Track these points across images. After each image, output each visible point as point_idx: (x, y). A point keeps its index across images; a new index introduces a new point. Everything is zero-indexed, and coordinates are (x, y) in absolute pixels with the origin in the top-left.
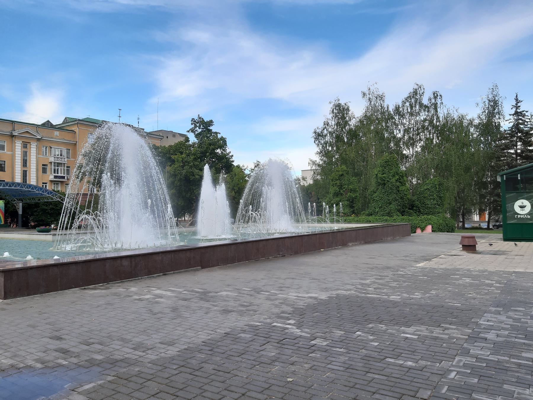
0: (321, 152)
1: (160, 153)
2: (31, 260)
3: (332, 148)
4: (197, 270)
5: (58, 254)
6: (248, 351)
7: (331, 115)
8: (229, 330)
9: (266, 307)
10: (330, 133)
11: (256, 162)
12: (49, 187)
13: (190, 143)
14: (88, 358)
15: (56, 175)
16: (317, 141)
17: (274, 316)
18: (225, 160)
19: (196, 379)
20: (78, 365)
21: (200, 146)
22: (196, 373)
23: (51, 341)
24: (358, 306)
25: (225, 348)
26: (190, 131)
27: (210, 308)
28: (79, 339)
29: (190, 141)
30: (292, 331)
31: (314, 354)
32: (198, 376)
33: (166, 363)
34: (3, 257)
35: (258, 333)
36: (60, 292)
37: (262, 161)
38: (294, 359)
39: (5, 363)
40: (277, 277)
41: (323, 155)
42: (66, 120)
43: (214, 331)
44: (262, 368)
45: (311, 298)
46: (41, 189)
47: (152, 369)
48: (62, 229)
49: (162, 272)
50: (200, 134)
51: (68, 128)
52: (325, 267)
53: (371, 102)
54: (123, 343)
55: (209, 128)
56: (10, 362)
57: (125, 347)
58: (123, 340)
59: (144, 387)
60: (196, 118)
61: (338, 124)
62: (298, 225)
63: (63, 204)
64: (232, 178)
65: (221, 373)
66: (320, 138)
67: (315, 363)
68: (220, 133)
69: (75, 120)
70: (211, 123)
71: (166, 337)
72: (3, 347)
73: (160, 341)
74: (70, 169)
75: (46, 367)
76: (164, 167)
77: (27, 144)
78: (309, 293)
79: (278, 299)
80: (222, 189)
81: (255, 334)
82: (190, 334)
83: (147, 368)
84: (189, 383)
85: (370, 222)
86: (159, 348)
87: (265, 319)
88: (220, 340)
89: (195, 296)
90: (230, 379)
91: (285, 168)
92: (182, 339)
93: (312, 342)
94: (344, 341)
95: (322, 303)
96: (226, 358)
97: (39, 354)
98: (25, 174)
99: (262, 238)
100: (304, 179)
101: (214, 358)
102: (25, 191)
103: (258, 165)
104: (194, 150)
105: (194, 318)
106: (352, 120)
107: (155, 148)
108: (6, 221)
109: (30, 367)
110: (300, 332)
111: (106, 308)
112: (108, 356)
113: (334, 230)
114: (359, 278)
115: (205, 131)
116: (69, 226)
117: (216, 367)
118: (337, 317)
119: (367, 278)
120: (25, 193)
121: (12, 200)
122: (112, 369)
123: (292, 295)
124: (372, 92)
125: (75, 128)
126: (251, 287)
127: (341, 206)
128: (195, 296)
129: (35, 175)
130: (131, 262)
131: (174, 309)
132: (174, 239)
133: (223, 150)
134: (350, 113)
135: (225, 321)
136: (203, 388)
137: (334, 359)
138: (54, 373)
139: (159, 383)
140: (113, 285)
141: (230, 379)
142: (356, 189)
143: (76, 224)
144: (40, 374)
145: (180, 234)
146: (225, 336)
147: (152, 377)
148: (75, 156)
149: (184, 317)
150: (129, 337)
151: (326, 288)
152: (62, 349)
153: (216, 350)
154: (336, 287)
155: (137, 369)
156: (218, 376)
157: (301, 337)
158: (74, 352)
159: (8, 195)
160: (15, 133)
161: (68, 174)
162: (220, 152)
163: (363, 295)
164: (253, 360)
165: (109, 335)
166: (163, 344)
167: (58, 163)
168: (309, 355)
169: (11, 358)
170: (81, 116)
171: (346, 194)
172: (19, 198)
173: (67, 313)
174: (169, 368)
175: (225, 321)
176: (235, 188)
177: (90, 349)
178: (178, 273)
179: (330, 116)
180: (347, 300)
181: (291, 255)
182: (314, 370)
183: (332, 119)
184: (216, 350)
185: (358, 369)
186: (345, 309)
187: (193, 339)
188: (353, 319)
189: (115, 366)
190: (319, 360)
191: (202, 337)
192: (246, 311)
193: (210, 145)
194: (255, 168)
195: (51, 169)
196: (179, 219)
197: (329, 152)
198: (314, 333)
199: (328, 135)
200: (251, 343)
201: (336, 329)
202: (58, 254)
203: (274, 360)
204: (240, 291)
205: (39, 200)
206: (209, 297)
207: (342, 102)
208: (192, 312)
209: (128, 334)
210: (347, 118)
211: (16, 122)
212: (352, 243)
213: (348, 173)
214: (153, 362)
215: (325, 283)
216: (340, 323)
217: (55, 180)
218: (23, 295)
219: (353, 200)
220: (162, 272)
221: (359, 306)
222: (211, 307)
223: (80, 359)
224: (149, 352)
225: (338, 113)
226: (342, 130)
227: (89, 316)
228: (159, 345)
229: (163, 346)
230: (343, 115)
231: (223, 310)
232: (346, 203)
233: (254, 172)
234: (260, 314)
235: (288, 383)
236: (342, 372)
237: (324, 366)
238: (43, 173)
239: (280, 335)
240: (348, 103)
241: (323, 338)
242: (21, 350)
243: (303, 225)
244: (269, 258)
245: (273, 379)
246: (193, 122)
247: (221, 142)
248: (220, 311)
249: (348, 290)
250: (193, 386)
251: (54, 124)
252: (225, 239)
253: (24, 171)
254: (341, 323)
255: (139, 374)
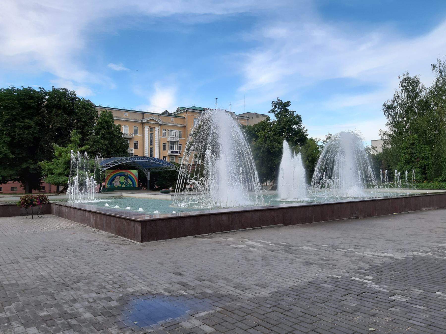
0: (392, 123)
1: (247, 131)
2: (157, 214)
3: (402, 118)
4: (281, 227)
5: (175, 210)
6: (330, 300)
7: (401, 88)
8: (312, 280)
9: (344, 262)
10: (400, 105)
11: (327, 134)
12: (168, 160)
13: (271, 122)
14: (201, 291)
15: (172, 150)
16: (386, 113)
17: (352, 271)
18: (300, 134)
19: (287, 318)
20: (195, 296)
21: (279, 123)
22: (287, 313)
23: (174, 276)
24: (436, 267)
25: (309, 295)
26: (271, 112)
27: (294, 259)
28: (194, 275)
29: (271, 120)
30: (371, 286)
31: (394, 309)
32: (289, 316)
33: (261, 302)
34: (139, 211)
35: (338, 285)
36: (178, 238)
37: (333, 134)
38: (375, 311)
39: (144, 290)
40: (352, 236)
41: (393, 126)
42: (179, 109)
43: (299, 279)
44: (345, 316)
45: (387, 257)
46: (162, 161)
47: (250, 305)
48: (178, 191)
49: (252, 227)
50: (279, 113)
51: (180, 115)
52: (399, 230)
53: (442, 73)
54: (227, 282)
55: (286, 108)
56: (148, 289)
57: (228, 285)
58: (226, 279)
59: (245, 319)
60: (276, 100)
61: (408, 96)
62: (370, 190)
63: (178, 173)
64: (306, 150)
65: (308, 316)
66: (390, 110)
67: (396, 317)
68: (296, 112)
69: (185, 109)
70: (288, 103)
71: (259, 280)
72: (142, 278)
73: (255, 283)
74: (182, 146)
75: (172, 295)
76: (250, 142)
77: (152, 129)
78: (385, 253)
79: (355, 256)
80: (299, 158)
81: (336, 285)
82: (279, 280)
83: (247, 304)
84: (281, 320)
85: (444, 188)
86: (255, 289)
87: (344, 273)
88: (305, 287)
89: (280, 248)
90: (316, 322)
91: (356, 139)
92: (272, 283)
93: (392, 298)
94: (424, 299)
95: (398, 262)
96: (311, 303)
97: (166, 285)
98: (151, 150)
99: (336, 202)
100: (374, 148)
101: (301, 303)
102: (152, 163)
103: (330, 137)
104: (274, 127)
105: (281, 267)
106: (423, 92)
107: (243, 127)
108: (139, 185)
109: (161, 294)
110: (378, 287)
111: (212, 253)
112: (216, 291)
113: (406, 195)
114: (435, 241)
115: (283, 111)
116: (183, 189)
117: (303, 310)
118: (415, 276)
119: (443, 241)
120: (152, 164)
121: (143, 170)
122: (219, 302)
123: (368, 254)
124: (442, 64)
125: (185, 115)
126: (328, 244)
127: (413, 172)
128: (280, 248)
129: (158, 151)
130: (229, 217)
131: (264, 258)
132: (259, 200)
133: (299, 126)
134: (420, 85)
135: (308, 272)
136: (293, 326)
137: (414, 315)
138: (178, 300)
139: (257, 318)
140: (216, 235)
141: (316, 322)
142: (428, 156)
143: (188, 187)
144: (168, 300)
145: (265, 196)
146: (309, 285)
147: (251, 312)
148: (185, 136)
149: (272, 265)
150: (230, 278)
151: (402, 249)
152: (182, 282)
153: (302, 295)
154: (413, 249)
155: (239, 304)
156: (306, 318)
157: (380, 292)
158: (191, 286)
159: (140, 166)
160: (144, 121)
161: (180, 149)
162: (296, 128)
163: (441, 257)
164: (335, 308)
165: (215, 274)
166: (258, 286)
167: (174, 142)
168: (389, 309)
169: (148, 286)
170: (188, 105)
171: (418, 162)
172: (147, 168)
173: (184, 255)
174: (264, 306)
175: (308, 272)
176: (309, 158)
177: (202, 285)
178: (265, 228)
179: (400, 90)
180: (424, 261)
181: (364, 217)
182: (395, 323)
183: (402, 92)
184: (302, 295)
185: (441, 327)
186: (423, 270)
187: (282, 284)
188: (432, 279)
189: (222, 300)
190: (400, 315)
191: (289, 283)
192: (325, 265)
193: (287, 122)
194: (326, 140)
195: (169, 146)
196: (262, 184)
197: (398, 121)
198: (392, 289)
199: (399, 107)
200: (333, 293)
201: (415, 288)
202: (175, 210)
203: (355, 311)
204: (319, 247)
205: (161, 169)
206: (292, 250)
207: (412, 76)
208: (279, 261)
209: (230, 275)
210: (418, 90)
211: (144, 112)
212: (426, 208)
213: (419, 142)
214: (250, 300)
215: (400, 244)
216: (418, 282)
217: (171, 154)
218: (154, 240)
219: (425, 167)
220: (252, 227)
221: (437, 267)
222: (294, 258)
223: (196, 291)
224: (247, 291)
225: (408, 86)
226: (413, 102)
227: (200, 258)
228: (255, 287)
229: (258, 288)
230: (413, 88)
231: (305, 262)
232: (418, 170)
233: (326, 144)
234: (339, 268)
235: (371, 332)
236: (424, 329)
237: (405, 320)
238: (163, 149)
239: (359, 288)
240: (418, 76)
241: (402, 294)
242: (154, 281)
243: (375, 190)
244: (343, 219)
245: (356, 327)
246: (273, 104)
247: (297, 119)
248: (302, 263)
249: (425, 252)
250: (284, 324)
251: (170, 113)
252: (303, 202)
253: (150, 148)
254: (420, 283)
255: (240, 308)
